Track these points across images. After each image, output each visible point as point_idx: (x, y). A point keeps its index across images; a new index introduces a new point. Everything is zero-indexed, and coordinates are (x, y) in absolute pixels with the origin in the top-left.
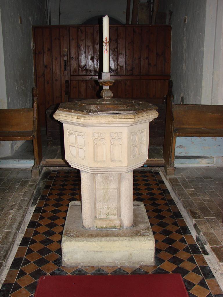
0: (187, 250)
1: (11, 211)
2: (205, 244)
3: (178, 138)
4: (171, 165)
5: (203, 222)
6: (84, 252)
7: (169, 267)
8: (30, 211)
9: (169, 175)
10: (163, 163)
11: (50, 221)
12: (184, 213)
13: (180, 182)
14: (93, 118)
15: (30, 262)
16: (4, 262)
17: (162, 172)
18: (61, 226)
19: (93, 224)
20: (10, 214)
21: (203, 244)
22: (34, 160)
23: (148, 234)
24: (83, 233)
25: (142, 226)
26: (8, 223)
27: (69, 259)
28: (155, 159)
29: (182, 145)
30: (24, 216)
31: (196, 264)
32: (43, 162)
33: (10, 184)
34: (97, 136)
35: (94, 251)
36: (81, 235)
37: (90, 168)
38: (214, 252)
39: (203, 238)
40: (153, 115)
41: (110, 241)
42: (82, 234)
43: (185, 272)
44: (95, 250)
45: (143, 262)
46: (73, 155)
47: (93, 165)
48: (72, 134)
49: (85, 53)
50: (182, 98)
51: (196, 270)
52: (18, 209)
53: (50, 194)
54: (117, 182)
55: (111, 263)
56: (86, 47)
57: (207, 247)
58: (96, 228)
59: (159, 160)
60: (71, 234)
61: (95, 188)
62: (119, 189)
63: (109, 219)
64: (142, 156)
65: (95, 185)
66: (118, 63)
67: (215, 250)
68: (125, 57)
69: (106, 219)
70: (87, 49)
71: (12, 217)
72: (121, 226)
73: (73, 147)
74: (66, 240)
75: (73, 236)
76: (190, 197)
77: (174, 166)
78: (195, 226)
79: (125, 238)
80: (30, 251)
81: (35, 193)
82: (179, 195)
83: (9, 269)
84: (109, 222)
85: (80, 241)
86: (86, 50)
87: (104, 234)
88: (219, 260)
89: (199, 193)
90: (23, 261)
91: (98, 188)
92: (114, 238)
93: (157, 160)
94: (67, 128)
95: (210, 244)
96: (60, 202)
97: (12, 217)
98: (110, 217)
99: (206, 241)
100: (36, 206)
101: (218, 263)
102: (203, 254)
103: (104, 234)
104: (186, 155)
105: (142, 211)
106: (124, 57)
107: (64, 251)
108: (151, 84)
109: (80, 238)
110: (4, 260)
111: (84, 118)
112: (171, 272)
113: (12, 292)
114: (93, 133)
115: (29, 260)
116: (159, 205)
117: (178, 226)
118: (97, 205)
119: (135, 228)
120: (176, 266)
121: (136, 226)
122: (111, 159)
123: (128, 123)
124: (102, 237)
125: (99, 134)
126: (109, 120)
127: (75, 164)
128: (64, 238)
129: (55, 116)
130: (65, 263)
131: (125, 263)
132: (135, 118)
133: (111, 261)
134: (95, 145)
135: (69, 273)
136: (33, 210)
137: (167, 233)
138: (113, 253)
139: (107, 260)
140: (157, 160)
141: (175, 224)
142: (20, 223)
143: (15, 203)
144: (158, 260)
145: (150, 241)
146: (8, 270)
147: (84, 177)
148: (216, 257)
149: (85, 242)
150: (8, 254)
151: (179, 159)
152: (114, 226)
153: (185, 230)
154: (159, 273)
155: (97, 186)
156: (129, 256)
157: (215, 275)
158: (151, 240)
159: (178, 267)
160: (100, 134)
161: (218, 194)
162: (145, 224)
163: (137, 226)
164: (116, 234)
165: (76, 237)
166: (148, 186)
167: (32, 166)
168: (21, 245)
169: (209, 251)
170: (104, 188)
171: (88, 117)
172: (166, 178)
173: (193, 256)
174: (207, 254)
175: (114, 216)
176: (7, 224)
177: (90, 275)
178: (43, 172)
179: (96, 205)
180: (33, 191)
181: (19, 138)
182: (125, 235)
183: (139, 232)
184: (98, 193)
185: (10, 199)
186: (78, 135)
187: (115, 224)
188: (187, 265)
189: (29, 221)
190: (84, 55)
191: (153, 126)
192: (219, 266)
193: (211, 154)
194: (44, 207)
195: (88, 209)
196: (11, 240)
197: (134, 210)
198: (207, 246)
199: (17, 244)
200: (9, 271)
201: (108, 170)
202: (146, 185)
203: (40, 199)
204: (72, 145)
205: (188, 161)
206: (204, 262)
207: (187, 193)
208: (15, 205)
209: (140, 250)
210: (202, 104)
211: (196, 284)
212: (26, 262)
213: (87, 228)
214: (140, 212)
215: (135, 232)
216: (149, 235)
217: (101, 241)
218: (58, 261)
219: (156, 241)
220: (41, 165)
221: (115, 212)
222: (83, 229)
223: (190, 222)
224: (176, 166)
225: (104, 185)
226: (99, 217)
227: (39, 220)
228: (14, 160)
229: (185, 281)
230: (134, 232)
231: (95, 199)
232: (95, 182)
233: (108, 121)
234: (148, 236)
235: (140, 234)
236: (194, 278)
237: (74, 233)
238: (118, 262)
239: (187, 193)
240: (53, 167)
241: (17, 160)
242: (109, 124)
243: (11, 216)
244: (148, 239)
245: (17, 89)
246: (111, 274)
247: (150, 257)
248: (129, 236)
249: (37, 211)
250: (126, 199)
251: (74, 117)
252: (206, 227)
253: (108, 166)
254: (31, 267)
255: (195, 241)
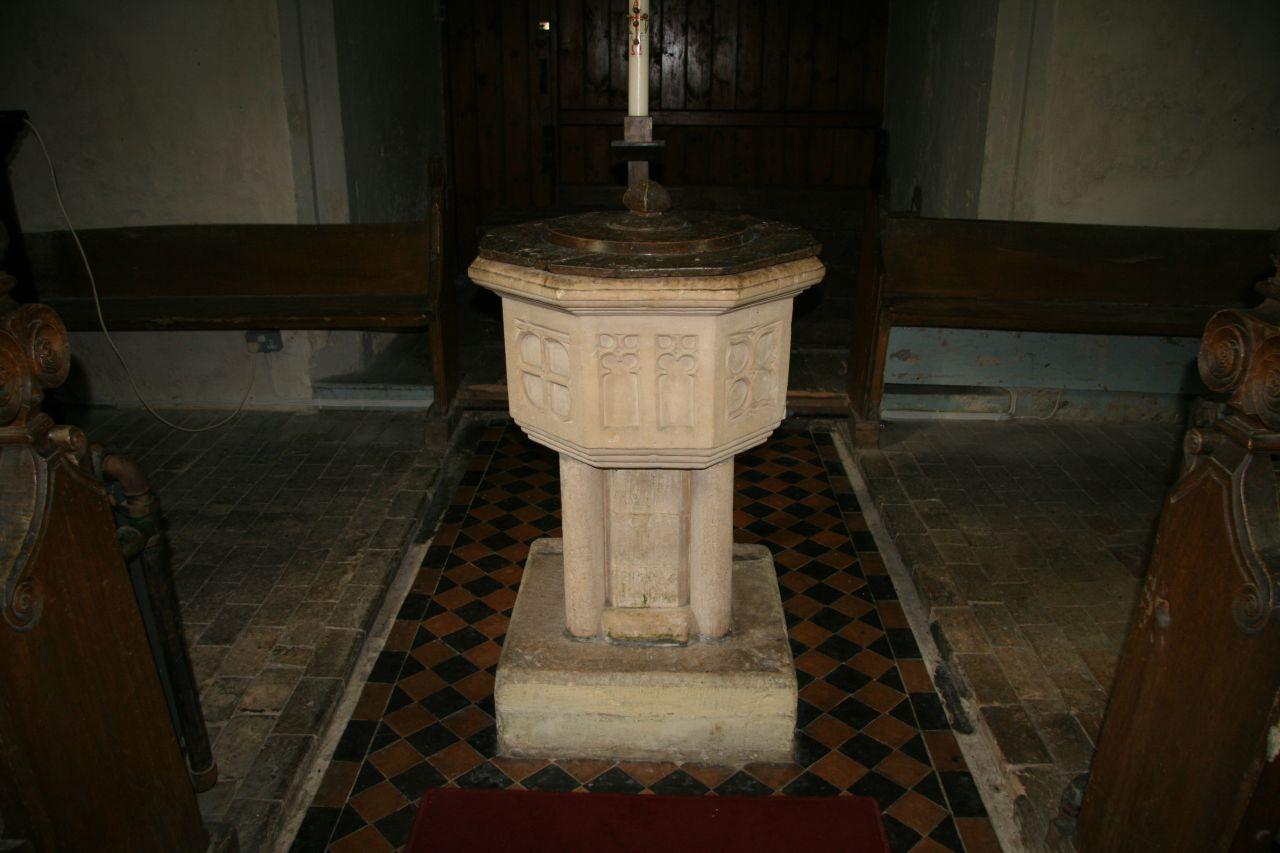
0: (902, 712)
1: (351, 560)
2: (964, 696)
3: (894, 330)
4: (871, 413)
5: (961, 618)
6: (568, 715)
7: (840, 771)
8: (411, 560)
9: (861, 448)
10: (846, 404)
11: (469, 598)
12: (902, 585)
13: (896, 474)
14: (597, 286)
15: (398, 737)
16: (315, 737)
17: (840, 433)
18: (504, 613)
19: (599, 625)
20: (345, 573)
21: (959, 695)
22: (432, 387)
23: (778, 664)
24: (565, 655)
25: (758, 635)
26: (338, 602)
27: (518, 737)
28: (818, 391)
29: (908, 351)
30: (389, 580)
31: (930, 765)
32: (461, 396)
33: (354, 464)
34: (610, 344)
35: (600, 714)
36: (557, 661)
37: (588, 451)
38: (990, 725)
39: (960, 674)
40: (807, 273)
41: (653, 686)
42: (564, 660)
43: (893, 792)
44: (602, 712)
45: (756, 752)
46: (533, 403)
47: (596, 440)
48: (529, 334)
49: (608, 35)
50: (918, 190)
51: (927, 788)
52: (373, 554)
53: (478, 502)
54: (680, 496)
55: (653, 752)
56: (609, 14)
57: (970, 707)
58: (607, 638)
59: (833, 394)
60: (528, 658)
61: (608, 510)
62: (684, 517)
63: (651, 611)
64: (767, 406)
65: (608, 501)
66: (712, 70)
67: (993, 719)
68: (735, 51)
69: (641, 611)
70: (612, 24)
71: (350, 582)
72: (692, 635)
73: (535, 378)
74: (509, 676)
75: (531, 665)
76: (927, 527)
77: (879, 416)
78: (935, 630)
79: (703, 677)
80: (400, 700)
81: (430, 496)
82: (891, 520)
83: (331, 757)
84: (651, 620)
85: (554, 684)
86: (610, 27)
87: (642, 641)
88: (1005, 756)
89: (955, 515)
90: (376, 732)
91: (617, 511)
92: (665, 677)
93: (824, 394)
94: (513, 314)
95: (981, 698)
96: (507, 532)
97: (350, 582)
98: (656, 604)
99: (966, 684)
100: (429, 543)
101: (1000, 764)
102: (954, 731)
103: (642, 641)
104: (919, 382)
105: (765, 580)
106: (732, 52)
107: (502, 710)
108: (805, 165)
109: (555, 673)
110: (314, 729)
111: (567, 287)
112: (844, 792)
113: (333, 840)
114: (599, 336)
115: (392, 732)
116: (824, 550)
117: (882, 629)
118: (614, 566)
119: (731, 644)
120: (864, 770)
121: (738, 635)
122: (658, 422)
123: (717, 304)
124: (627, 671)
125: (617, 339)
126: (653, 295)
127: (543, 433)
128: (502, 670)
129: (471, 274)
130: (507, 747)
131: (699, 753)
132: (741, 288)
133: (654, 746)
134: (604, 376)
135: (518, 783)
136: (422, 557)
137: (841, 648)
138: (660, 721)
139: (642, 743)
140: (824, 394)
141: (871, 619)
142: (378, 604)
143: (363, 532)
144: (807, 744)
145: (782, 690)
146: (328, 762)
147: (573, 481)
148: (996, 742)
149: (570, 684)
150: (331, 710)
151: (898, 396)
152: (667, 635)
153: (907, 647)
154: (812, 789)
155: (612, 507)
156: (712, 734)
157: (989, 806)
158: (785, 686)
159: (871, 776)
160: (622, 337)
161: (1016, 517)
162: (770, 629)
163: (743, 633)
164: (674, 660)
165: (542, 668)
166: (782, 494)
167: (427, 403)
168: (375, 676)
169: (975, 718)
170: (637, 512)
171: (580, 282)
172: (851, 454)
173: (923, 737)
174: (969, 731)
175: (669, 601)
176: (333, 605)
177: (584, 790)
178: (462, 425)
179: (609, 564)
180: (426, 494)
181: (383, 319)
182: (701, 668)
183: (747, 656)
184: (615, 525)
185: (351, 517)
186: (550, 340)
187: (670, 629)
188: (900, 769)
189: (406, 594)
190: (604, 42)
191: (805, 305)
192: (1004, 773)
193: (1001, 381)
194: (454, 548)
195: (584, 578)
196: (341, 661)
197: (735, 575)
198: (971, 703)
199: (362, 674)
200: (330, 765)
201: (649, 457)
202: (785, 477)
203: (444, 520)
204: (528, 369)
205: (926, 400)
206: (957, 757)
207: (916, 511)
208: (363, 539)
209: (750, 716)
210: (980, 217)
211: (925, 835)
212: (387, 737)
213: (581, 637)
214: (757, 583)
215: (735, 655)
216: (780, 669)
217: (622, 684)
218: (487, 739)
219: (803, 679)
220: (456, 403)
221: (673, 588)
222: (567, 642)
223: (917, 620)
224: (885, 415)
225: (637, 503)
226: (620, 605)
227: (436, 594)
228: (371, 386)
229: (892, 821)
230: (733, 659)
231: (607, 544)
232: (608, 491)
233: (646, 297)
234: (777, 671)
235: (752, 662)
236: (916, 812)
237: (536, 653)
238: (676, 749)
239: (916, 511)
240: (494, 409)
241: (382, 386)
242: (651, 308)
243: (349, 577)
244: (776, 683)
245: (382, 154)
246: (652, 792)
247: (781, 739)
248: (713, 671)
249: (432, 560)
250: (708, 552)
251: (533, 280)
252: (973, 636)
253: (648, 446)
254: (399, 757)
255: (933, 681)
